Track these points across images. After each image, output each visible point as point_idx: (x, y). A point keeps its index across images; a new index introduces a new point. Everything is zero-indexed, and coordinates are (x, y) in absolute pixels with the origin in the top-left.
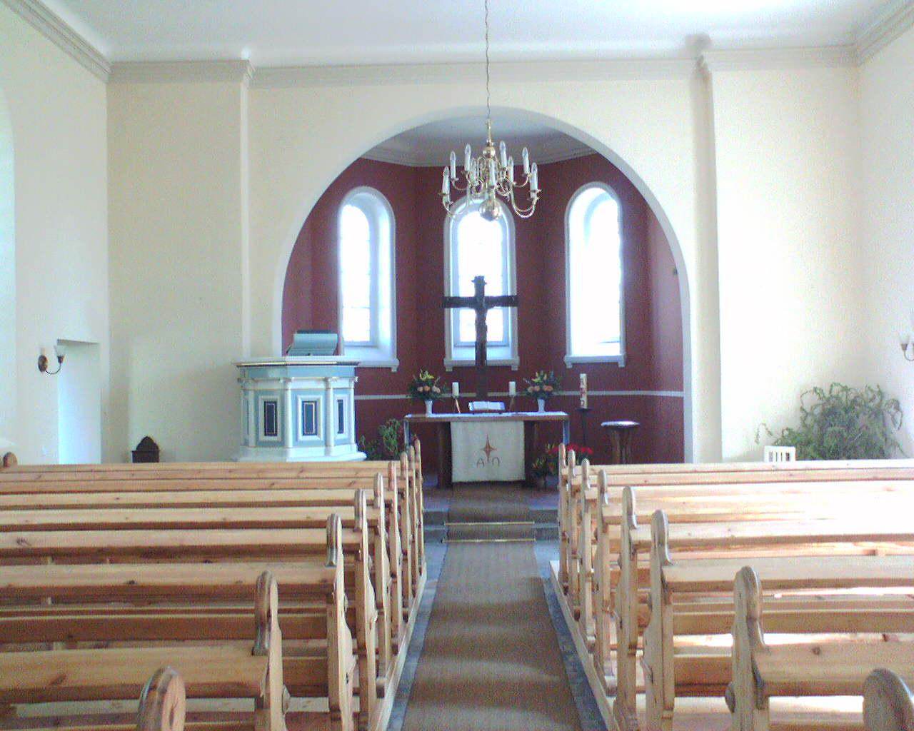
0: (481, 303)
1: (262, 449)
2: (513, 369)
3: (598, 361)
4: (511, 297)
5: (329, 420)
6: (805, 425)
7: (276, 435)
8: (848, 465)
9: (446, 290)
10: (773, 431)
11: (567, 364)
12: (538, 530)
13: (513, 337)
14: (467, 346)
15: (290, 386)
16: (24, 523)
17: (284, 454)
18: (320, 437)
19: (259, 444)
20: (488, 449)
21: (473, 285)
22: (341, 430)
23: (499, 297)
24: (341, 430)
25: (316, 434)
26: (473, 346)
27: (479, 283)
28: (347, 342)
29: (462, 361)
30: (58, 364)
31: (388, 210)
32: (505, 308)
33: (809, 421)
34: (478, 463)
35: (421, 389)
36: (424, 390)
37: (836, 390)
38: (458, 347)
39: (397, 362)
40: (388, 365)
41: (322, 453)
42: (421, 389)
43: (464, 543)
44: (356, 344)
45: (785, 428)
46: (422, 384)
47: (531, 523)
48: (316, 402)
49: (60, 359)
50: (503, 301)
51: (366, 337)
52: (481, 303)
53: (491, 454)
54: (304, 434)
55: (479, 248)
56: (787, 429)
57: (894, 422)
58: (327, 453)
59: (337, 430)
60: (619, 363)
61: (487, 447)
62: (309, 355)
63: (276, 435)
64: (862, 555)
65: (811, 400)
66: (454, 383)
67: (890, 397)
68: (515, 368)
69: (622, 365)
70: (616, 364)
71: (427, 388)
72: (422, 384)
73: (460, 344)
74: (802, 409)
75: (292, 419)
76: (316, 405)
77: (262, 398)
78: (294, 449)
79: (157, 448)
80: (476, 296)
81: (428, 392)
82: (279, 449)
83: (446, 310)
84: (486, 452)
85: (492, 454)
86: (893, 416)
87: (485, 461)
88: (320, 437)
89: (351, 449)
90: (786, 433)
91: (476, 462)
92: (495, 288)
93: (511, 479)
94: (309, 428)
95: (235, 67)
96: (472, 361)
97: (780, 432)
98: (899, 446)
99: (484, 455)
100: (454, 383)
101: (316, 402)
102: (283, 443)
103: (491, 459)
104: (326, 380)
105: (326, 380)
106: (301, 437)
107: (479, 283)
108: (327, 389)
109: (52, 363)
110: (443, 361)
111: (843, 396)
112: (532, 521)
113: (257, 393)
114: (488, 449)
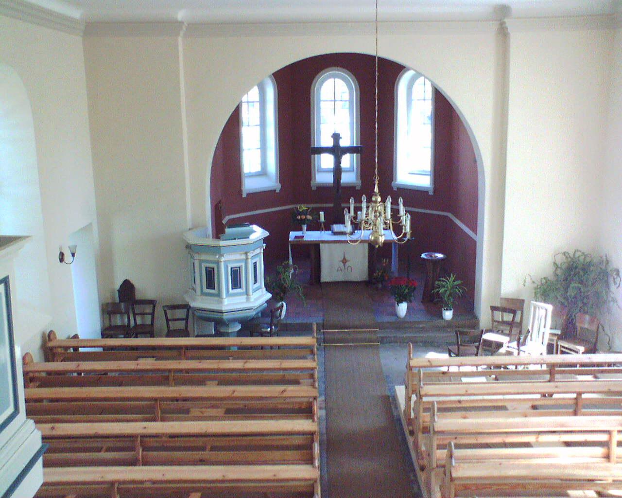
0: (337, 151)
1: (204, 297)
2: (357, 189)
3: (416, 189)
4: (356, 147)
5: (249, 288)
6: (556, 275)
7: (214, 289)
8: (589, 358)
9: (312, 144)
10: (535, 281)
11: (394, 188)
12: (382, 337)
13: (357, 164)
14: (327, 171)
15: (223, 259)
16: (100, 480)
17: (221, 302)
18: (242, 289)
19: (203, 294)
20: (344, 261)
21: (332, 139)
22: (256, 281)
23: (338, 78)
24: (256, 281)
25: (240, 288)
26: (330, 171)
27: (336, 137)
28: (247, 173)
29: (323, 184)
30: (72, 258)
31: (272, 81)
32: (352, 155)
33: (559, 272)
34: (338, 270)
35: (299, 217)
36: (301, 218)
37: (578, 254)
38: (320, 172)
39: (280, 186)
40: (273, 188)
41: (245, 300)
42: (299, 217)
43: (336, 347)
44: (253, 174)
45: (543, 277)
46: (300, 213)
47: (376, 330)
48: (240, 268)
49: (73, 255)
50: (351, 150)
51: (257, 168)
52: (337, 151)
53: (346, 264)
54: (232, 289)
55: (335, 109)
56: (545, 278)
57: (615, 283)
58: (248, 299)
59: (253, 282)
60: (430, 192)
61: (343, 260)
62: (235, 239)
63: (214, 289)
64: (600, 458)
65: (560, 259)
66: (321, 213)
67: (615, 267)
68: (358, 188)
69: (431, 193)
70: (427, 192)
71: (303, 217)
72: (300, 213)
73: (322, 170)
74: (555, 263)
75: (224, 278)
76: (240, 269)
77: (204, 265)
78: (227, 299)
79: (134, 286)
80: (333, 146)
81: (304, 219)
82: (216, 298)
83: (312, 156)
84: (343, 262)
85: (347, 264)
86: (614, 279)
87: (343, 268)
88: (242, 289)
89: (262, 292)
90: (544, 281)
91: (336, 269)
92: (345, 142)
93: (359, 280)
94: (236, 284)
95: (170, 27)
96: (331, 183)
97: (539, 281)
98: (617, 302)
99: (342, 264)
100: (321, 213)
101: (240, 268)
102: (219, 295)
103: (346, 267)
104: (246, 253)
105: (246, 253)
106: (231, 291)
107: (336, 137)
108: (247, 259)
109: (68, 257)
110: (310, 183)
111: (582, 259)
112: (377, 328)
113: (201, 261)
114: (344, 261)
